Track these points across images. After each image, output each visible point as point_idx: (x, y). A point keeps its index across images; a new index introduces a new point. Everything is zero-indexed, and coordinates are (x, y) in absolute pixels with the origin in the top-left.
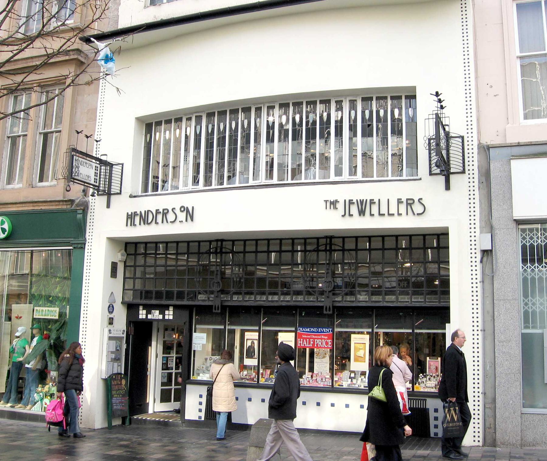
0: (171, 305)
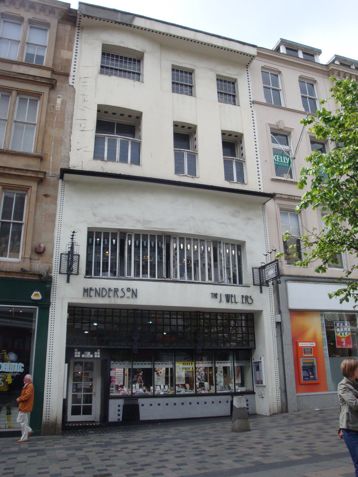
0: (76, 348)
